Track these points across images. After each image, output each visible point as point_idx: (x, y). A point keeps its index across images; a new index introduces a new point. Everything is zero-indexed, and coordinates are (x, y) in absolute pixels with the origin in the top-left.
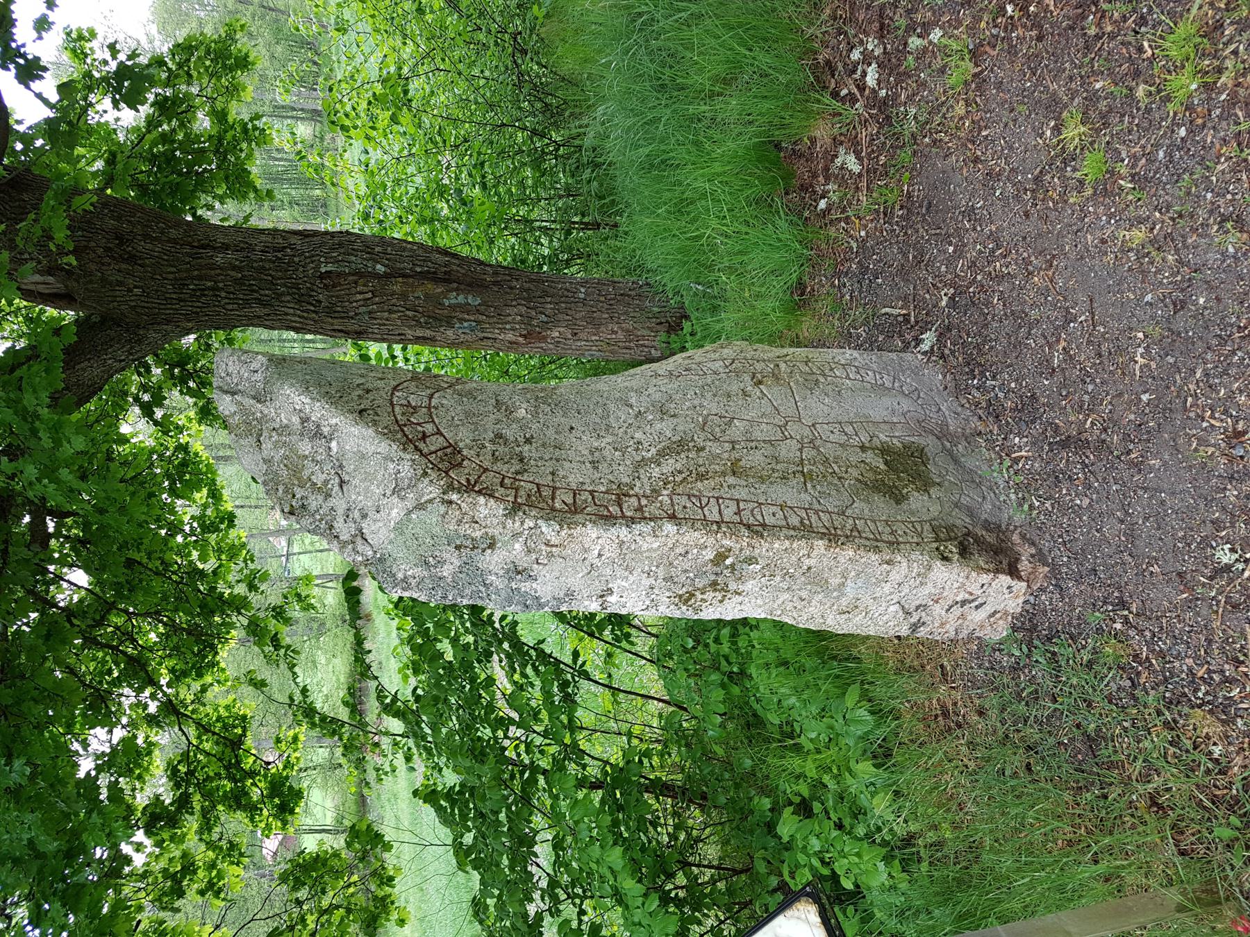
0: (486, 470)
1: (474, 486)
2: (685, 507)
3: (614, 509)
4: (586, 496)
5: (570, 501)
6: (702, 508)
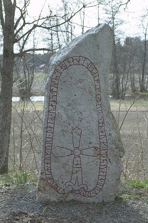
0: (61, 74)
1: (56, 71)
2: (51, 115)
3: (51, 99)
4: (56, 94)
5: (53, 90)
6: (51, 119)
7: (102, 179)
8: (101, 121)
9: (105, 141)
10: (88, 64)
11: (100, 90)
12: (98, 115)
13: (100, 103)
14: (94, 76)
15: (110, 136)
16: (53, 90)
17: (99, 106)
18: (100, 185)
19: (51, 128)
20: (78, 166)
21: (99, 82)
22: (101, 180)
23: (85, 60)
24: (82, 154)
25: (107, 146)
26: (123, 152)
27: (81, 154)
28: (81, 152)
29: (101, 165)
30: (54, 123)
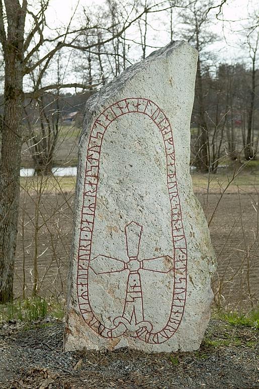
0: (106, 128)
6: (89, 207)
7: (177, 312)
8: (175, 211)
9: (183, 246)
10: (153, 111)
12: (171, 200)
13: (174, 179)
14: (164, 131)
15: (192, 237)
16: (93, 157)
17: (172, 185)
18: (175, 322)
19: (88, 222)
20: (137, 289)
21: (172, 143)
22: (175, 313)
23: (149, 104)
24: (143, 268)
25: (187, 254)
26: (214, 266)
27: (140, 268)
28: (142, 264)
29: (176, 287)
30: (94, 215)
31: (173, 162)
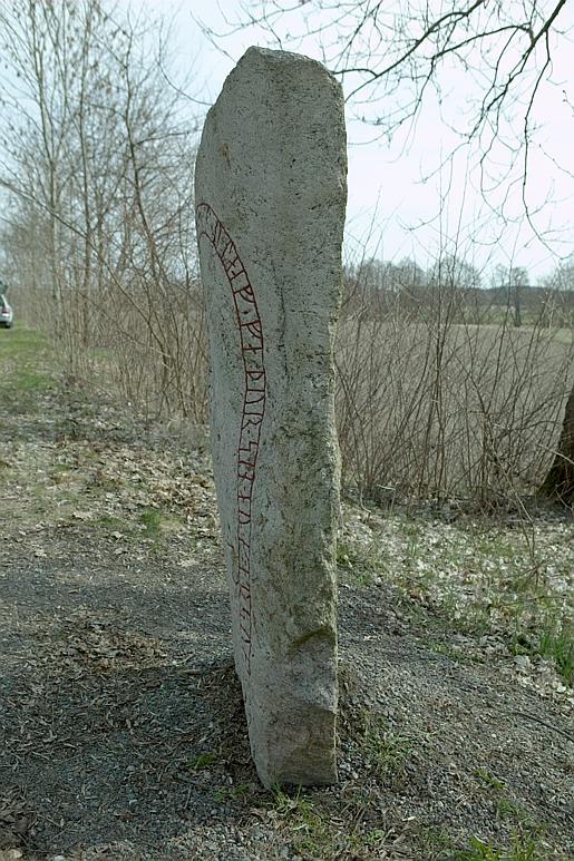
11: (261, 332)
13: (260, 384)
21: (251, 298)
31: (256, 342)
